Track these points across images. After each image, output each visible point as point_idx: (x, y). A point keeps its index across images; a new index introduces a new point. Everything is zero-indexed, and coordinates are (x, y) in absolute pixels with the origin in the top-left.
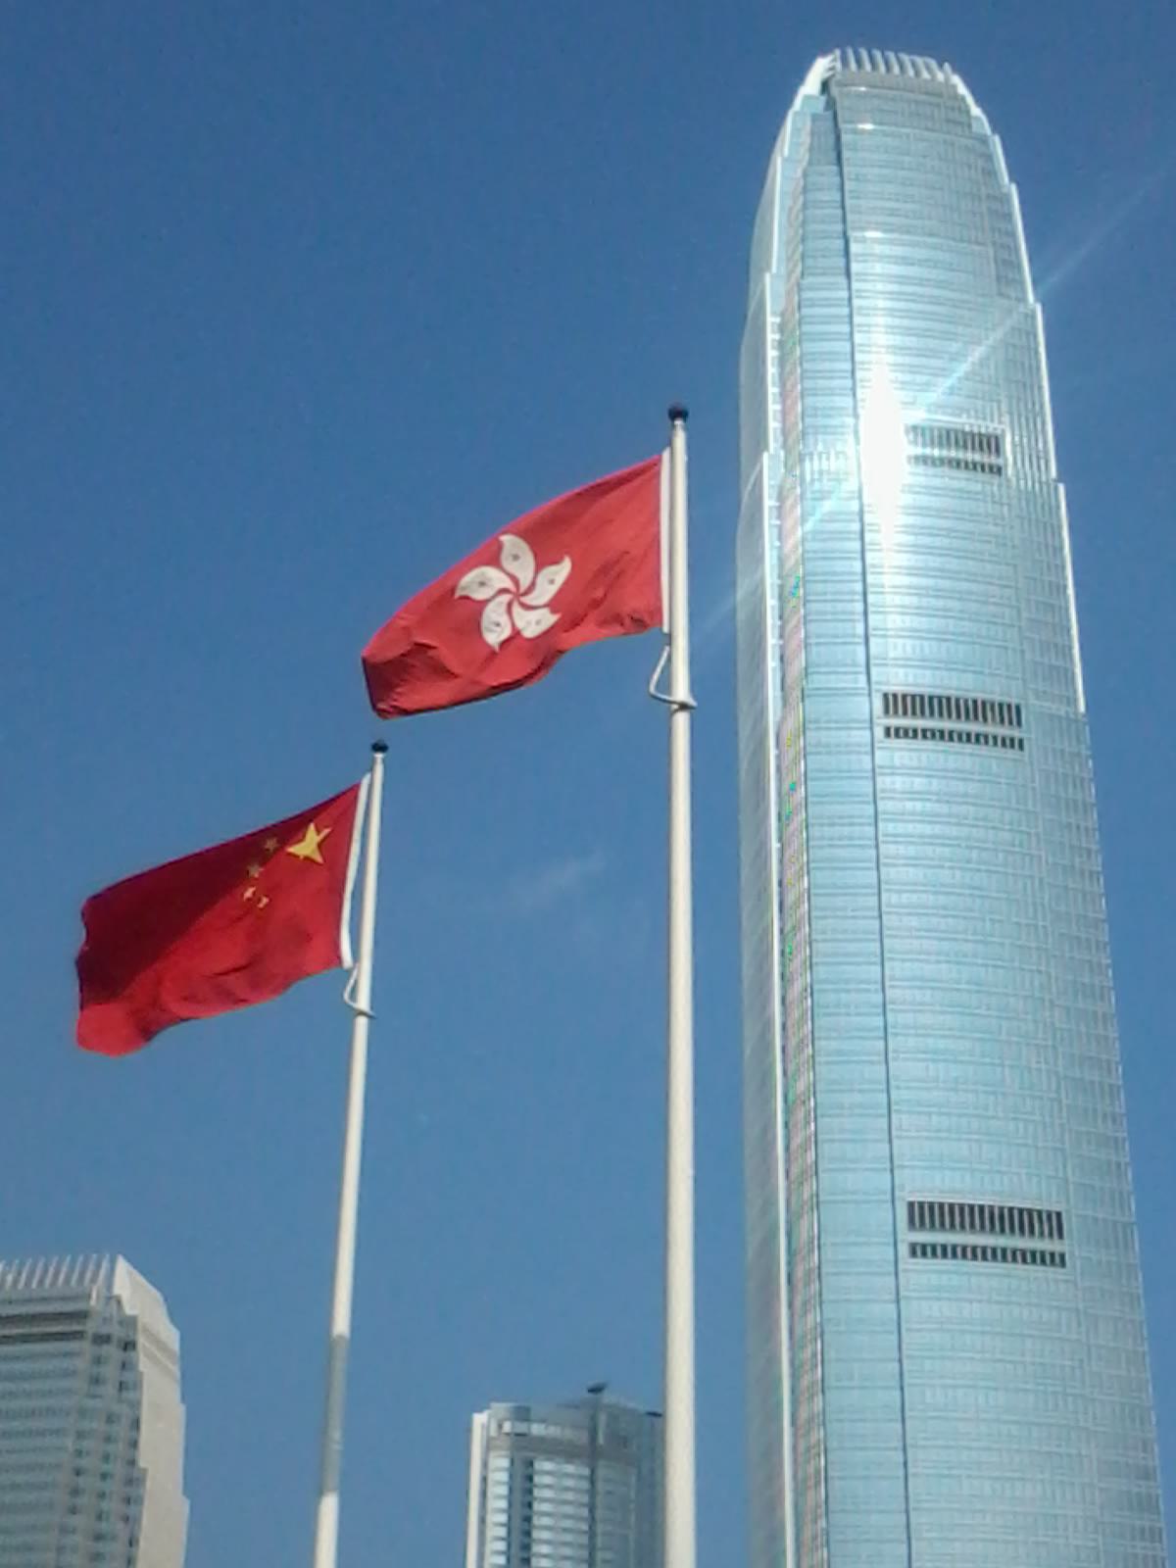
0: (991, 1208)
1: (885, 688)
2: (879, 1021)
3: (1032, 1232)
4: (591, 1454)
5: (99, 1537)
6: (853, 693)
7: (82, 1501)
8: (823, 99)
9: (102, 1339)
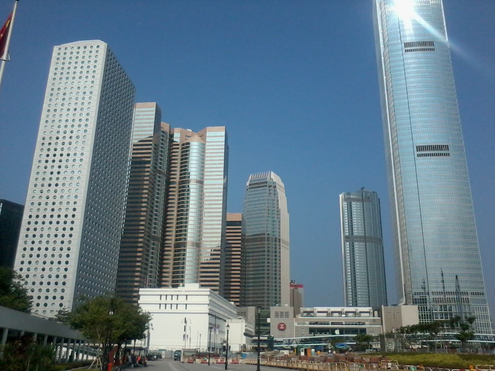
0: (433, 146)
1: (404, 42)
2: (406, 91)
4: (363, 201)
5: (273, 221)
6: (399, 44)
7: (270, 215)
9: (270, 186)
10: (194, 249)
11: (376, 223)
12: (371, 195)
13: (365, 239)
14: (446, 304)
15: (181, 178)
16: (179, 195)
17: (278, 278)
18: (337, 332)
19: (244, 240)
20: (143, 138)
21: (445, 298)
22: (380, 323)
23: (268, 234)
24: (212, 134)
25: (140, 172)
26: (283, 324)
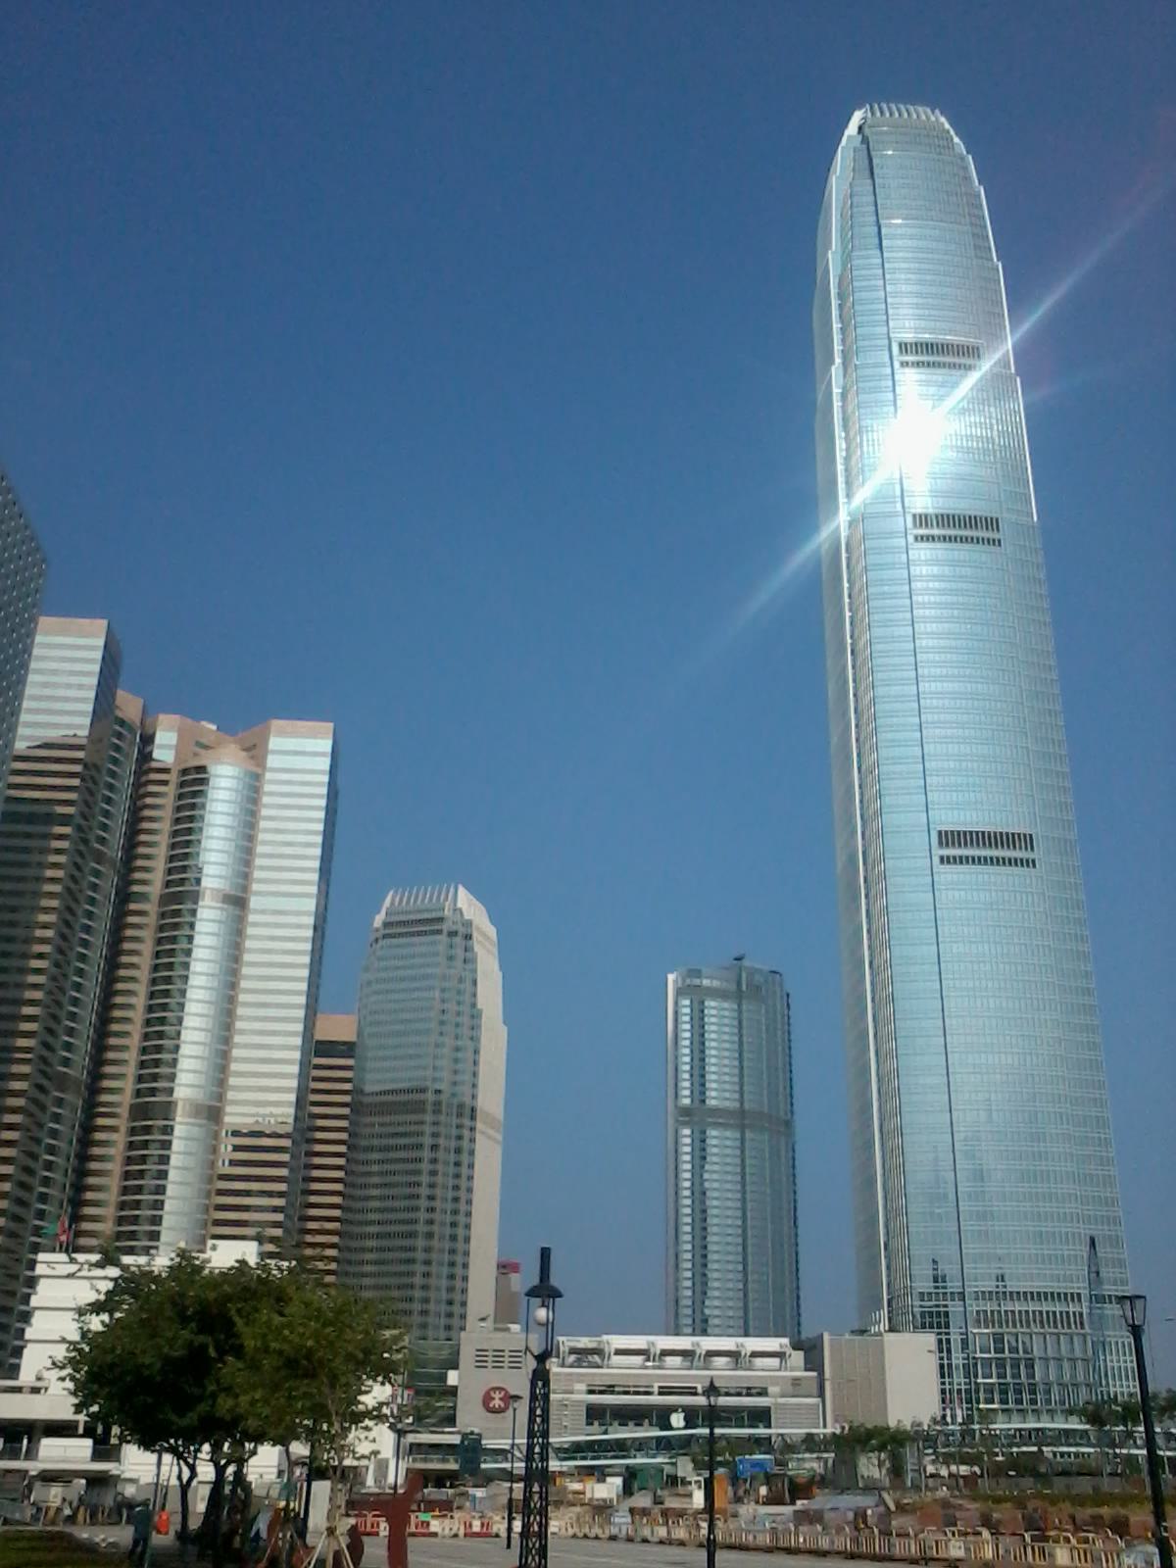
0: (989, 833)
1: (913, 511)
2: (913, 674)
3: (1015, 847)
4: (739, 996)
8: (860, 137)
9: (452, 934)
10: (200, 1126)
11: (777, 1069)
12: (766, 981)
13: (739, 1119)
14: (1000, 1330)
15: (168, 884)
16: (159, 941)
17: (460, 1238)
18: (677, 1420)
19: (358, 1108)
20: (53, 734)
21: (999, 1312)
22: (815, 1391)
23: (438, 1092)
24: (290, 743)
25: (26, 850)
26: (500, 1389)
